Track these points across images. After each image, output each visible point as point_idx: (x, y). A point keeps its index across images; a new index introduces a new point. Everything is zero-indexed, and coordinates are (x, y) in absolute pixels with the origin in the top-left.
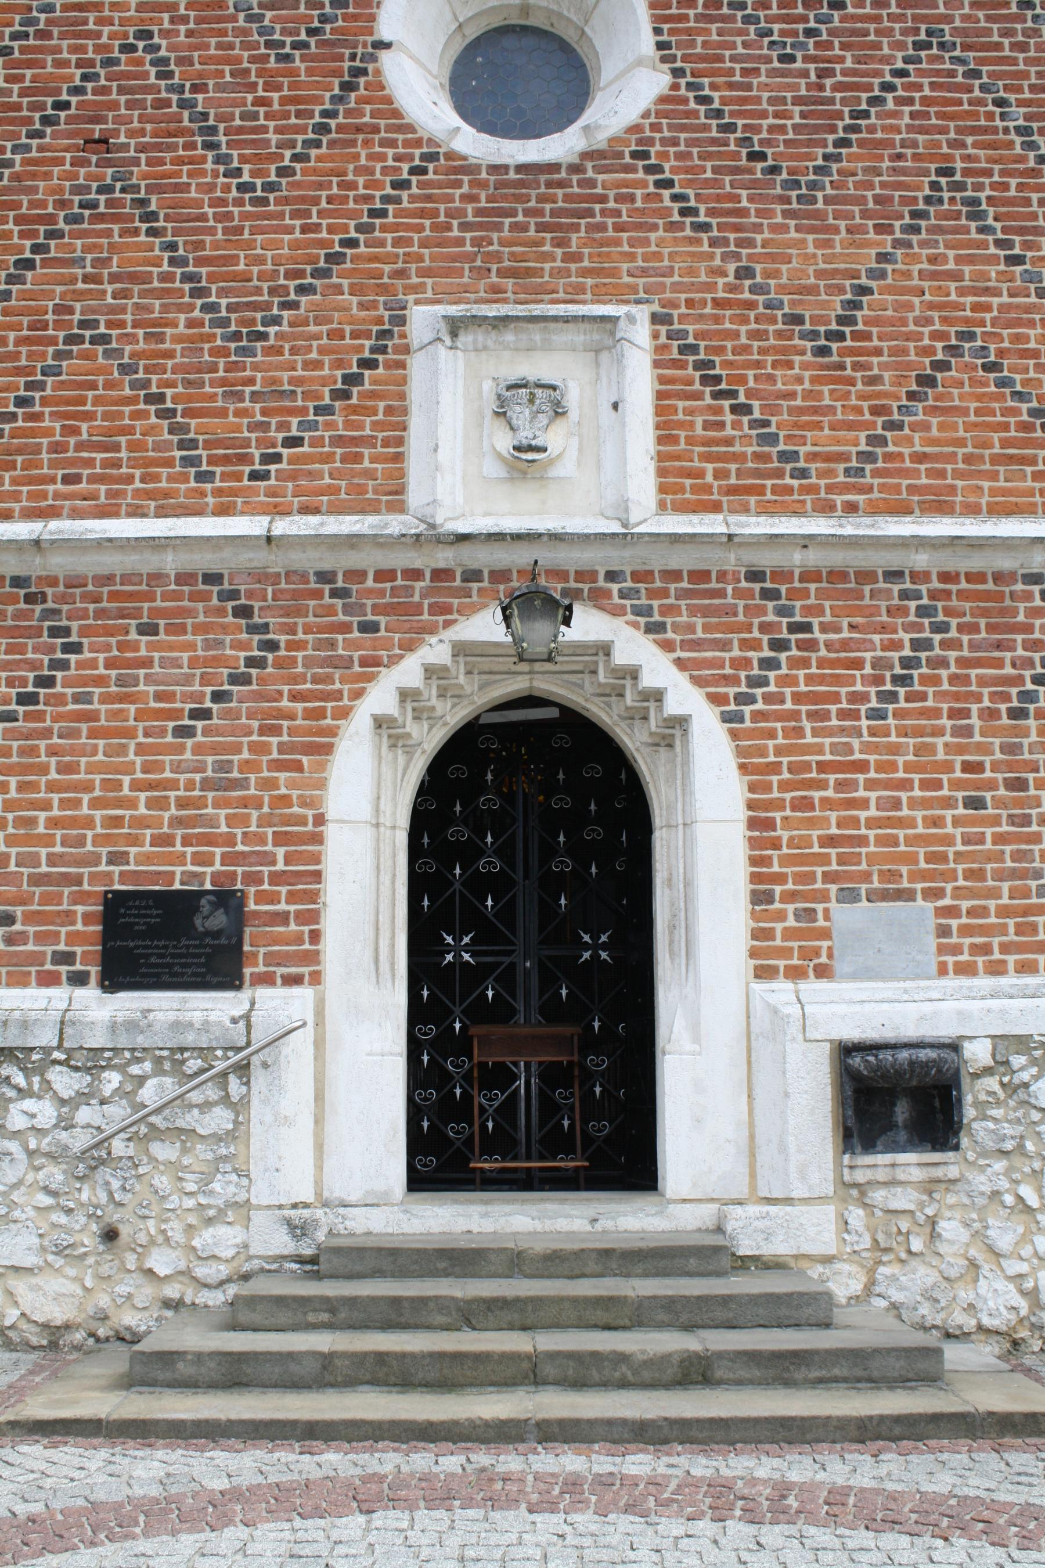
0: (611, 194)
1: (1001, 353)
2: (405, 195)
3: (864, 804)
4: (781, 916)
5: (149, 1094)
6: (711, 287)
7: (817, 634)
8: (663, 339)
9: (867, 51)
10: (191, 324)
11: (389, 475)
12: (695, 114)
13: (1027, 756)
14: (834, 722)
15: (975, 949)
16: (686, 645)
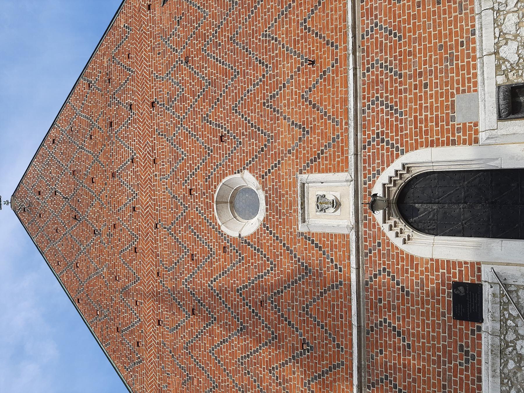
0: (272, 184)
1: (307, 88)
2: (273, 232)
3: (426, 116)
4: (459, 137)
5: (515, 313)
6: (293, 160)
7: (379, 131)
8: (306, 171)
9: (238, 125)
10: (303, 284)
11: (340, 238)
12: (253, 164)
13: (412, 72)
14: (403, 125)
15: (469, 82)
16: (383, 165)
